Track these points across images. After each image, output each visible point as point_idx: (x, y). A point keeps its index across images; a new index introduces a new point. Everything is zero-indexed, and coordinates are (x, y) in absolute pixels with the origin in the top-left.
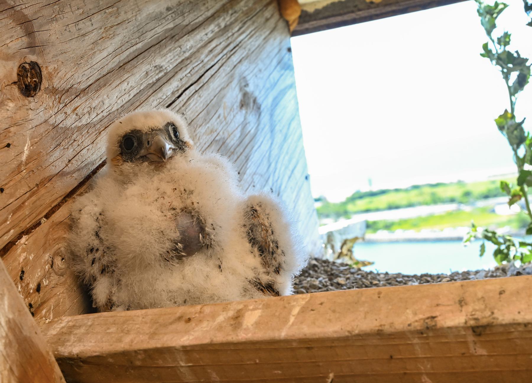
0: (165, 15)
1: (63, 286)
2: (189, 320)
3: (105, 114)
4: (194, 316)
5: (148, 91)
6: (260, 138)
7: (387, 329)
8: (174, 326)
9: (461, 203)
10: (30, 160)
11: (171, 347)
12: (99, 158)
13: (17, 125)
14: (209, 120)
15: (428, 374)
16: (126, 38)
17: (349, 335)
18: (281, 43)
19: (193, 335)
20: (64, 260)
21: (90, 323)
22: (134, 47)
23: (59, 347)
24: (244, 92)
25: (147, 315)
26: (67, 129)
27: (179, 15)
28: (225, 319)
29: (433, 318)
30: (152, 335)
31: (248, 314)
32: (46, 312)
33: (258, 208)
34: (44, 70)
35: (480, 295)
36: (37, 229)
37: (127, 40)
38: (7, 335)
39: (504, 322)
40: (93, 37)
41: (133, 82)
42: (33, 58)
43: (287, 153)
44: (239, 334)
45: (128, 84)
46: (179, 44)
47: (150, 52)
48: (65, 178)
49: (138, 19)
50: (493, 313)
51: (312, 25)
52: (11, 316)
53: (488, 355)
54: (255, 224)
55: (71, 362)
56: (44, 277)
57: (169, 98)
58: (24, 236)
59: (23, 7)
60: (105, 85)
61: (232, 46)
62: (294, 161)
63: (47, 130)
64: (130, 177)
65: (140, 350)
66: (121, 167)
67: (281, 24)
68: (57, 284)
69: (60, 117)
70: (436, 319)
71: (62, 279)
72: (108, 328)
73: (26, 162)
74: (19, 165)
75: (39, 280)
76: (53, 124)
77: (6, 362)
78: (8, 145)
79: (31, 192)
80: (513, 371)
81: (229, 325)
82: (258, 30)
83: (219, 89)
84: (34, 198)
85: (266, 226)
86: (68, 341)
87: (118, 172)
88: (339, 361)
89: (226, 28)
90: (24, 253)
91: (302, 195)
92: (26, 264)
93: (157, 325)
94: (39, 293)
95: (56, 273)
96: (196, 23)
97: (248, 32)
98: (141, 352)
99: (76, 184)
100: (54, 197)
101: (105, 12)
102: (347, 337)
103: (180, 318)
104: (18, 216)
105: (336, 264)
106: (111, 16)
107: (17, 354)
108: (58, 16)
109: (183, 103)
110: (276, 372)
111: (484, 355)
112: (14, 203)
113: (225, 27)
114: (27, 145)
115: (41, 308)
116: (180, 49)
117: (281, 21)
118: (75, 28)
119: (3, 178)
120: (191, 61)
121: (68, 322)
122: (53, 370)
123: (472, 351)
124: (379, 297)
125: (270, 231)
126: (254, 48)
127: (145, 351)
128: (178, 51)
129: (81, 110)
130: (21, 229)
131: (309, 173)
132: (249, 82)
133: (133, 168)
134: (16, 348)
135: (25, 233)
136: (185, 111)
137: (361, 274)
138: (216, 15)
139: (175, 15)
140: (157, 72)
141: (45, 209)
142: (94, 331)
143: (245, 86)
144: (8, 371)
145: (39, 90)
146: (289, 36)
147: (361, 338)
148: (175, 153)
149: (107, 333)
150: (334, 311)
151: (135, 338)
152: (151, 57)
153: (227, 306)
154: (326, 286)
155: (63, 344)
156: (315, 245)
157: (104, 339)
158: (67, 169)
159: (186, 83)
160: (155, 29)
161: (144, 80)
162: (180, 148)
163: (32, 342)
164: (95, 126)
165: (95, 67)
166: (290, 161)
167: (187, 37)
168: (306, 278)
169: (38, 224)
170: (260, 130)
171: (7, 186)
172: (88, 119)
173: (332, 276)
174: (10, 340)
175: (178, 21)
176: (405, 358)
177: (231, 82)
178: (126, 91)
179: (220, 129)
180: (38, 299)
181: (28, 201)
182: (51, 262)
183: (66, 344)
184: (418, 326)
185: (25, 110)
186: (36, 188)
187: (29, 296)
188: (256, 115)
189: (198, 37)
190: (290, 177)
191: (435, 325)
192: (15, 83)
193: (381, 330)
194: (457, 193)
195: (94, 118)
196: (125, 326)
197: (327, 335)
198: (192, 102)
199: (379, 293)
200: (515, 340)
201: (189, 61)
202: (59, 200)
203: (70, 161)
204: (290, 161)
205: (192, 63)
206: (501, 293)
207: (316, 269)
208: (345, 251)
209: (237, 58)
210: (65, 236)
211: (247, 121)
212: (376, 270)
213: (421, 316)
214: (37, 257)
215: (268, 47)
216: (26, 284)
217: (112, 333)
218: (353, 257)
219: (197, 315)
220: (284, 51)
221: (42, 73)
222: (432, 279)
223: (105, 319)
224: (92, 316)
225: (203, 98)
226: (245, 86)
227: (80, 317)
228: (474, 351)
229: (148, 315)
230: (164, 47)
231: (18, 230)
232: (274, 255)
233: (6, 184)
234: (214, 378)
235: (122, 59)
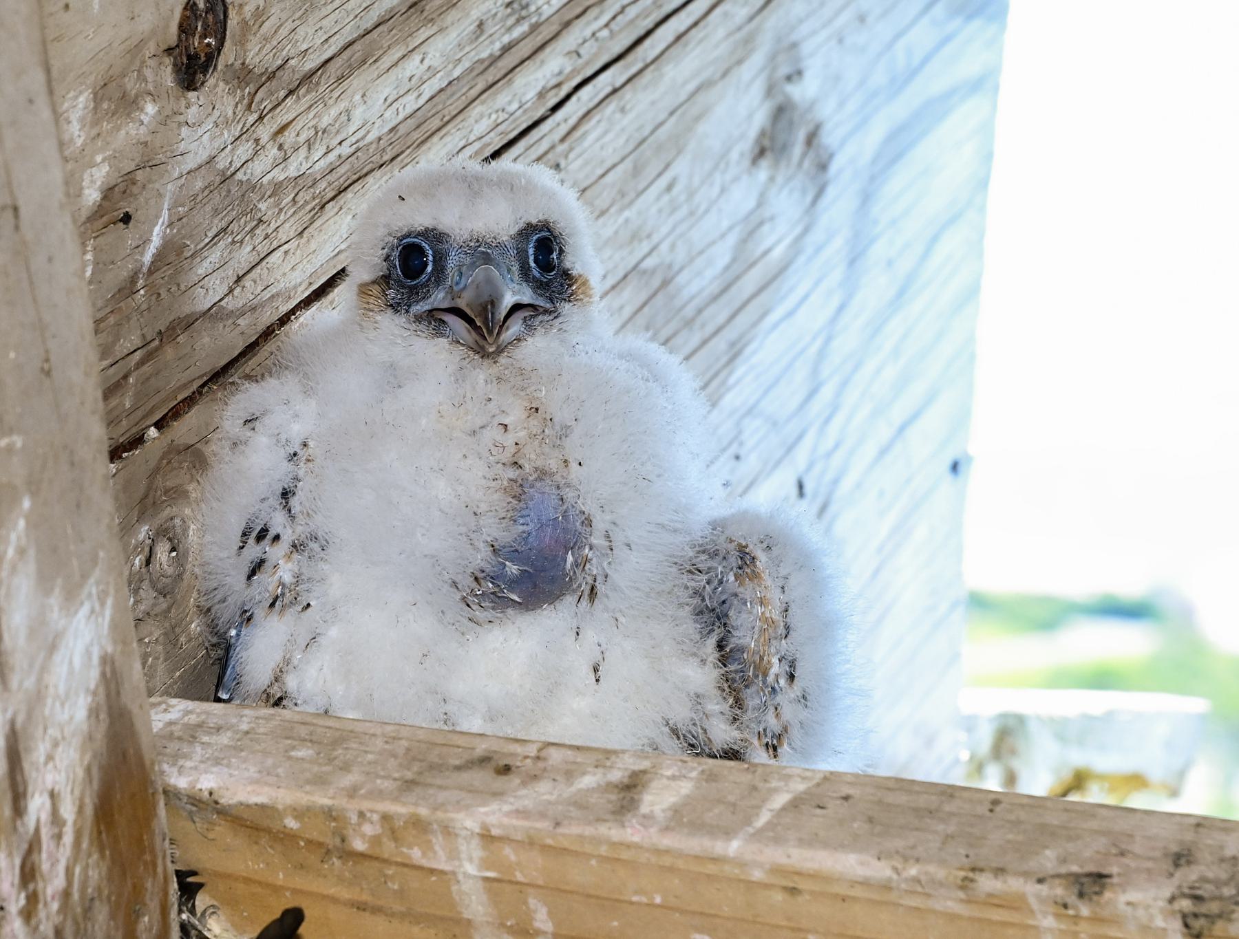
3: (346, 150)
4: (519, 764)
8: (466, 777)
20: (174, 554)
21: (244, 727)
24: (779, 99)
45: (422, 61)
52: (110, 649)
63: (209, 185)
72: (294, 748)
73: (150, 268)
76: (223, 172)
78: (126, 219)
83: (691, 87)
84: (146, 368)
86: (186, 757)
95: (153, 585)
109: (564, 129)
114: (161, 221)
129: (294, 134)
131: (971, 450)
143: (789, 78)
156: (929, 742)
159: (587, 63)
161: (467, 49)
179: (664, 230)
182: (147, 549)
183: (181, 762)
186: (157, 342)
188: (804, 191)
190: (884, 451)
213: (1075, 868)
225: (631, 116)
226: (789, 78)
229: (400, 739)
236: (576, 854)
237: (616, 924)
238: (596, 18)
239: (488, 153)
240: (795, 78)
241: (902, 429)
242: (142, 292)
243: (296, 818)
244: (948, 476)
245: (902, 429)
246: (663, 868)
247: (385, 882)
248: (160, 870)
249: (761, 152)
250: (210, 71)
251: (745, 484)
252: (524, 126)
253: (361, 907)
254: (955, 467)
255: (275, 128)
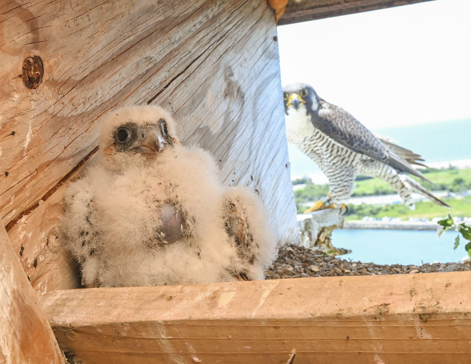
0: (156, 8)
1: (56, 263)
2: (171, 298)
3: (98, 104)
4: (175, 295)
5: (138, 81)
6: (242, 127)
7: (345, 313)
8: (157, 303)
9: (451, 191)
10: (31, 147)
11: (154, 321)
12: (92, 146)
13: (21, 114)
14: (194, 109)
15: (379, 354)
16: (120, 31)
17: (312, 317)
18: (267, 32)
19: (174, 312)
20: (58, 239)
21: (81, 297)
22: (127, 39)
23: (54, 317)
24: (229, 81)
25: (133, 293)
26: (63, 118)
27: (170, 8)
28: (203, 298)
29: (386, 305)
30: (138, 310)
31: (223, 295)
32: (41, 286)
33: (235, 203)
34: (46, 63)
35: (429, 286)
36: (35, 210)
37: (120, 33)
38: (12, 303)
39: (447, 311)
40: (90, 31)
41: (125, 74)
42: (36, 53)
43: (268, 141)
44: (214, 313)
45: (120, 75)
46: (169, 36)
47: (141, 45)
48: (61, 163)
49: (131, 13)
50: (438, 303)
51: (299, 14)
52: (15, 287)
53: (432, 340)
54: (232, 217)
55: (64, 330)
56: (41, 253)
57: (157, 89)
58: (24, 216)
59: (29, 5)
60: (99, 77)
61: (218, 36)
62: (275, 149)
63: (47, 119)
64: (123, 166)
65: (126, 323)
66: (114, 156)
67: (268, 13)
68: (51, 260)
69: (59, 107)
70: (388, 306)
71: (56, 256)
72: (98, 302)
73: (27, 149)
74: (22, 151)
75: (36, 256)
76: (52, 114)
77: (11, 327)
78: (13, 133)
79: (31, 176)
80: (454, 354)
81: (206, 304)
82: (244, 20)
83: (204, 79)
84: (33, 182)
85: (242, 220)
86: (62, 312)
87: (111, 161)
88: (303, 340)
89: (215, 18)
90: (24, 231)
91: (282, 183)
92: (25, 242)
93: (142, 301)
94: (36, 268)
95: (51, 251)
96: (185, 15)
97: (235, 22)
98: (127, 324)
99: (70, 169)
100: (51, 181)
101: (102, 8)
102: (310, 319)
103: (162, 296)
104: (20, 197)
105: (311, 252)
106: (107, 11)
107: (20, 320)
108: (60, 13)
109: (170, 93)
110: (246, 347)
111: (429, 339)
112: (17, 186)
113: (213, 17)
114: (29, 133)
115: (37, 282)
116: (169, 40)
117: (268, 9)
118: (74, 24)
119: (8, 163)
120: (179, 53)
121: (63, 295)
122: (49, 336)
123: (419, 335)
124: (340, 285)
125: (246, 226)
126: (240, 38)
127: (131, 324)
128: (168, 43)
129: (77, 100)
130: (22, 209)
131: (290, 161)
132: (233, 72)
133: (125, 158)
134: (19, 316)
135: (25, 213)
136: (172, 101)
137: (334, 262)
138: (204, 6)
139: (166, 7)
140: (147, 63)
141: (43, 191)
142: (85, 304)
143: (230, 75)
144: (12, 334)
145: (41, 83)
146: (275, 25)
147: (322, 320)
148: (166, 147)
149: (97, 306)
150: (300, 296)
151: (122, 312)
152: (142, 49)
153: (205, 287)
154: (300, 273)
155: (58, 314)
156: (292, 232)
157: (93, 312)
158: (63, 156)
159: (173, 74)
160: (147, 22)
161: (134, 72)
162: (170, 144)
163: (32, 310)
164: (89, 115)
165: (90, 60)
166: (271, 149)
167: (176, 29)
168: (281, 264)
169: (37, 205)
170: (243, 119)
171: (11, 170)
172: (83, 109)
173: (306, 263)
174: (14, 308)
175: (168, 14)
176: (361, 340)
177: (216, 72)
178: (118, 82)
179: (204, 117)
180: (35, 273)
181: (29, 184)
182: (46, 240)
183: (60, 314)
184: (372, 312)
185: (28, 101)
186: (36, 173)
187: (27, 270)
188: (239, 104)
189: (187, 28)
190: (270, 165)
191: (388, 312)
192: (20, 76)
193: (340, 314)
194: (448, 180)
195: (88, 107)
196: (114, 301)
197: (292, 317)
198: (179, 92)
199: (341, 282)
200: (456, 327)
201: (177, 52)
202: (55, 184)
203: (65, 148)
204: (271, 149)
205: (180, 54)
206: (447, 286)
207: (292, 255)
208: (322, 238)
209: (223, 48)
210: (59, 217)
211: (231, 110)
212: (349, 259)
213: (376, 303)
214: (35, 236)
215: (255, 37)
216: (24, 259)
217: (101, 306)
218: (330, 245)
219: (178, 294)
220: (270, 40)
221: (44, 67)
222: (401, 270)
223: (95, 293)
224: (83, 291)
225: (189, 88)
226: (230, 75)
227: (73, 291)
228: (421, 336)
229: (134, 292)
230: (154, 39)
231: (19, 210)
232: (249, 247)
233: (10, 168)
234: (191, 350)
235: (115, 52)
236: (198, 326)
237: (217, 347)
238: (173, 62)
239: (148, 100)
240: (231, 75)
241: (273, 159)
242: (26, 157)
243: (100, 328)
244: (286, 168)
245: (273, 159)
246: (230, 327)
247: (136, 345)
248: (56, 356)
249: (226, 95)
250: (40, 82)
251: (238, 180)
252: (157, 93)
253: (129, 354)
254: (286, 166)
255: (70, 99)
